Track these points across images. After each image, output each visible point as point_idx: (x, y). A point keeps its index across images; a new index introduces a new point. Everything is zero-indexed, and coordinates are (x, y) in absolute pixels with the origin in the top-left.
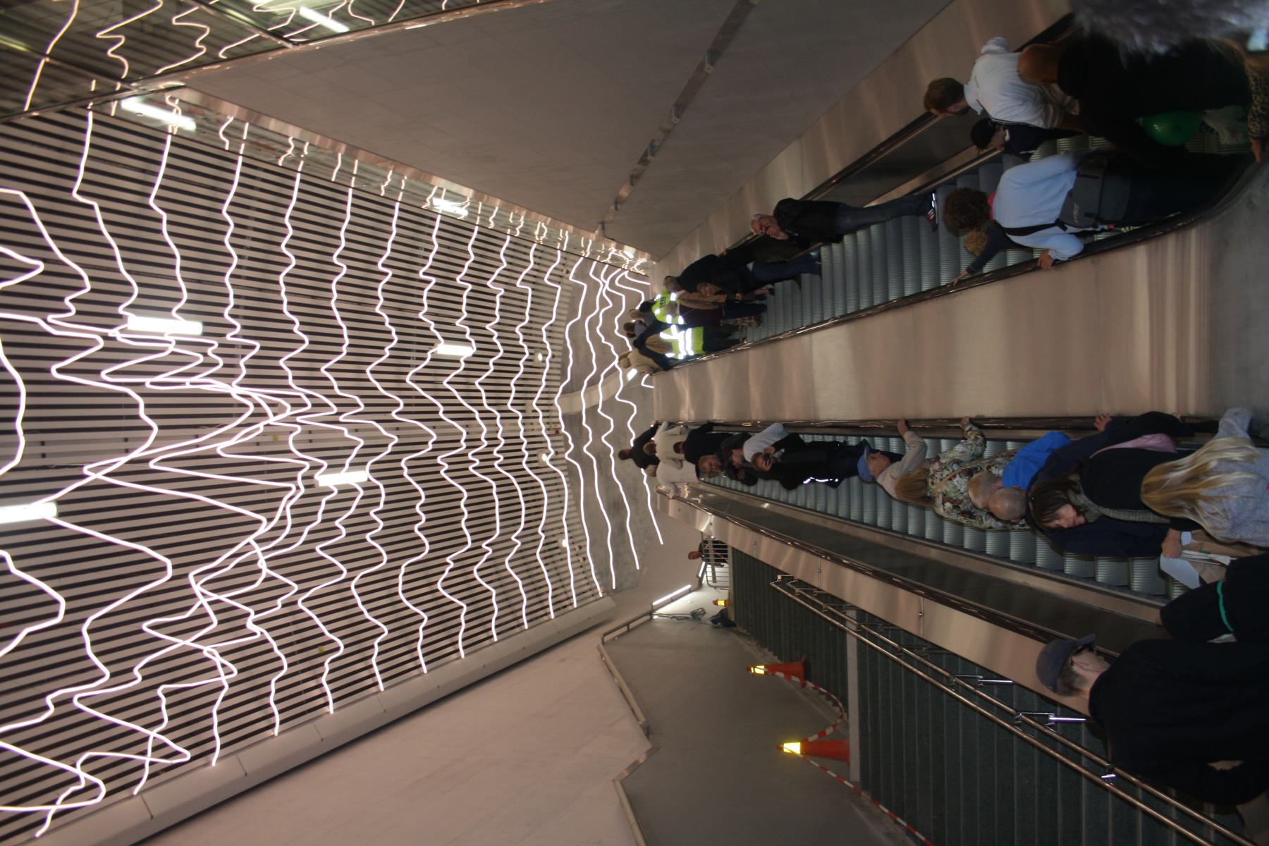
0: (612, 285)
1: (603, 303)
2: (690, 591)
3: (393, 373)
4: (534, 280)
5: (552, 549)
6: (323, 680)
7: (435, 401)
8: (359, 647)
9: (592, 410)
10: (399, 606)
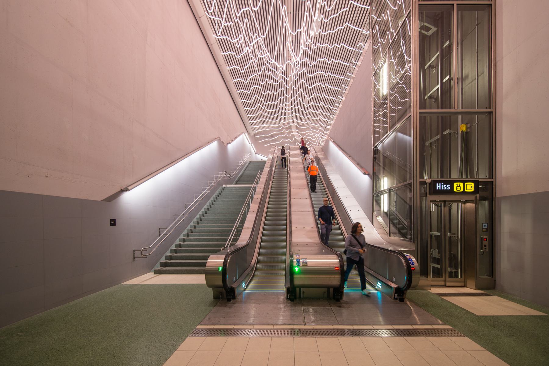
3: (302, 86)
5: (264, 122)
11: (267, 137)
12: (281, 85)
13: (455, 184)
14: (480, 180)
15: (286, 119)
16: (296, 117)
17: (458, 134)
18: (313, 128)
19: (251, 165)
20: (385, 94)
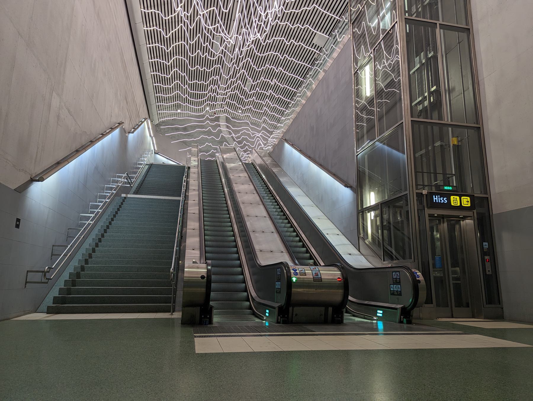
0: (258, 137)
1: (253, 134)
2: (154, 149)
3: (247, 67)
4: (265, 114)
5: (178, 106)
6: (155, 28)
7: (194, 41)
8: (163, 41)
9: (219, 126)
10: (175, 55)
11: (177, 129)
12: (219, 61)
13: (452, 197)
14: (476, 195)
15: (213, 107)
16: (229, 105)
17: (449, 147)
18: (252, 124)
19: (153, 169)
20: (368, 94)
